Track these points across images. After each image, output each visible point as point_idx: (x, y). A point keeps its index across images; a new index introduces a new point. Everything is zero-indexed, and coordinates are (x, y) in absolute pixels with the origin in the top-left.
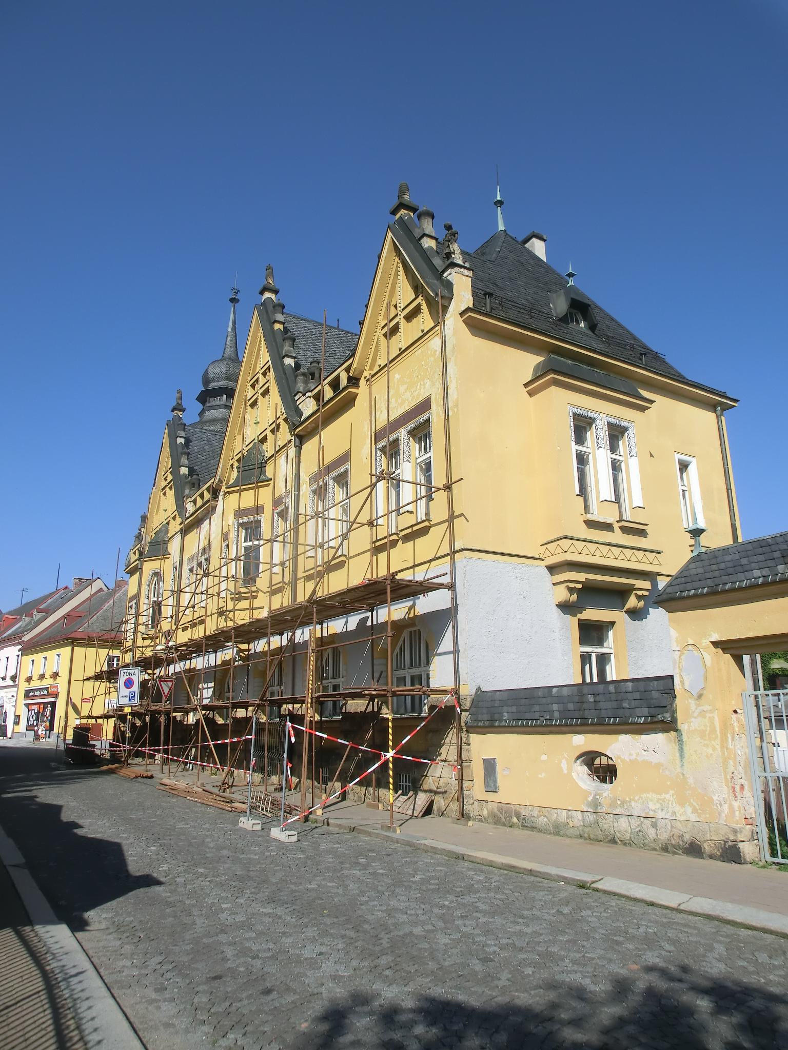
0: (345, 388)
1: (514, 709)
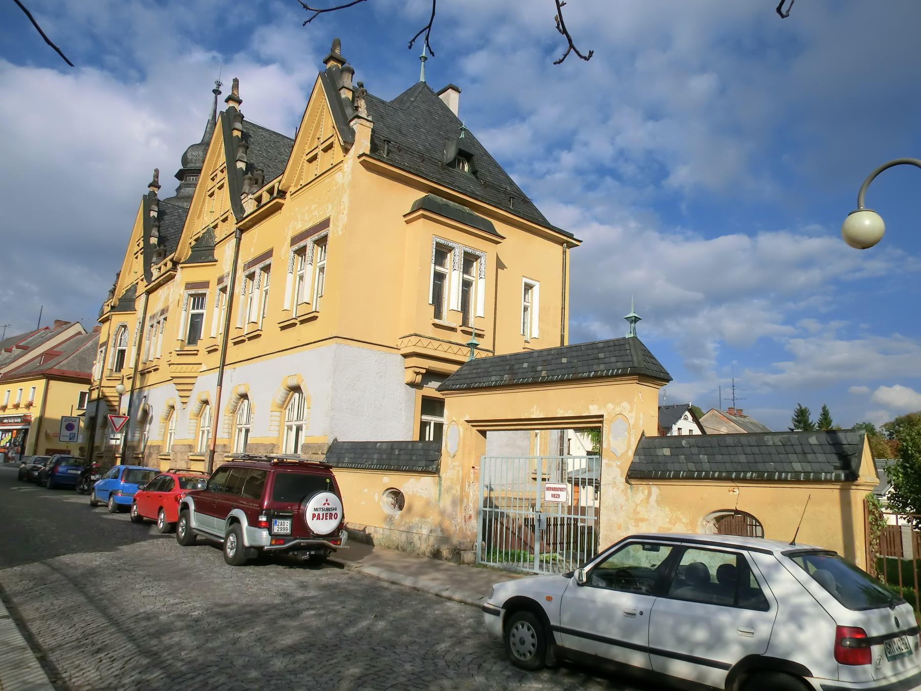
0: (276, 198)
1: (352, 455)
